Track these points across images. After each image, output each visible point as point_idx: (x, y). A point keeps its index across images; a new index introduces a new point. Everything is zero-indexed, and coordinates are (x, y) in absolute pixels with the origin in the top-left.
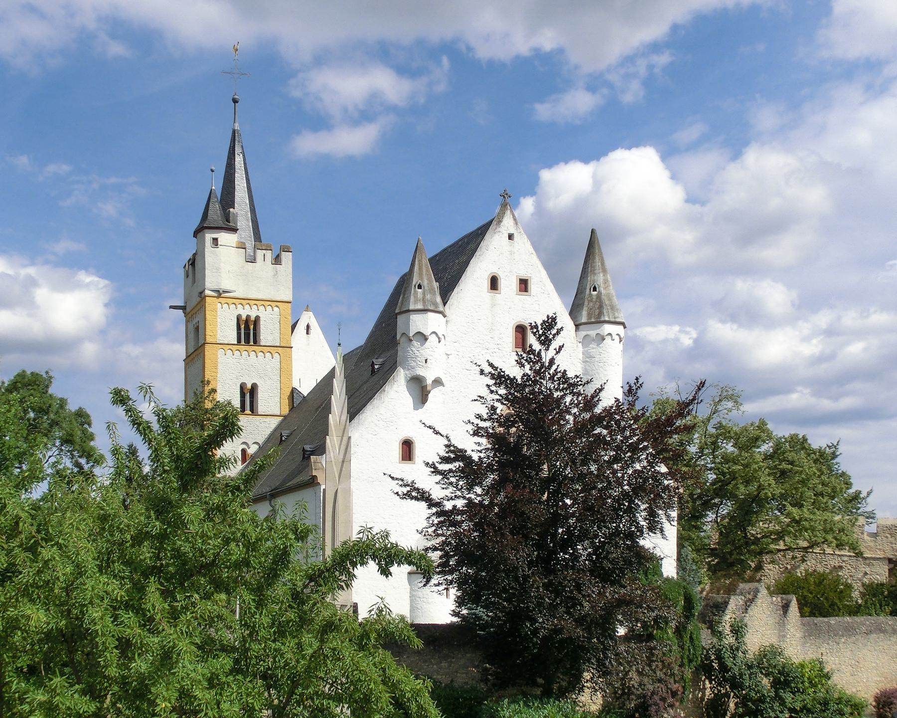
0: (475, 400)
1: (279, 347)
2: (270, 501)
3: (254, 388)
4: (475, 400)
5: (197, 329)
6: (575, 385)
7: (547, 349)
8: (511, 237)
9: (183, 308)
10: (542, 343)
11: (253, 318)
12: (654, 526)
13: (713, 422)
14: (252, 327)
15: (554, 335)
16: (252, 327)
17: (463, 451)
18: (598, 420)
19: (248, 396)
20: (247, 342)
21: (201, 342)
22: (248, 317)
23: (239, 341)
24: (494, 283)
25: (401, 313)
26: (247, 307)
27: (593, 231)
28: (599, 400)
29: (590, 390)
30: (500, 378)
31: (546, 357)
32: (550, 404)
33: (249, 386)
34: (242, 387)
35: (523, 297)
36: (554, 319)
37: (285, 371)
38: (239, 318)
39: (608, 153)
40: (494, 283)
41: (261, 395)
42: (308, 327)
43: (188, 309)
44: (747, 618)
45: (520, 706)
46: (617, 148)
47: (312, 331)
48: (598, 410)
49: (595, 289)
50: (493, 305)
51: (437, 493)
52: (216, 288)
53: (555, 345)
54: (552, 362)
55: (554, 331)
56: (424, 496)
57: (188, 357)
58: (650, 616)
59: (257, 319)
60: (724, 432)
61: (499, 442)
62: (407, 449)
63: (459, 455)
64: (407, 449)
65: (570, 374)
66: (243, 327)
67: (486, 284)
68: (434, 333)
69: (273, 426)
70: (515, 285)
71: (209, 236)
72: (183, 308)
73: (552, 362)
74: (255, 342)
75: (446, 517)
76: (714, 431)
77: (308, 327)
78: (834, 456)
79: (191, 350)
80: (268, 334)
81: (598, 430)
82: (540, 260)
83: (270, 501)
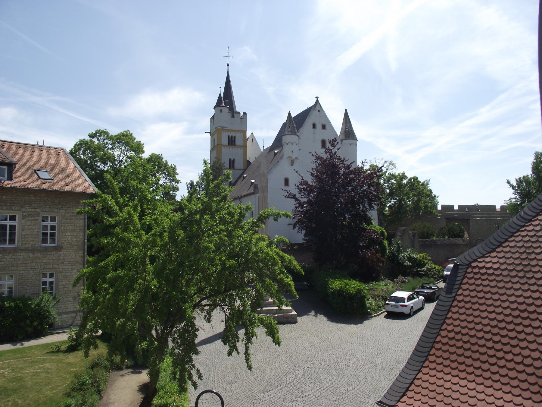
0: (247, 360)
3: (234, 160)
4: (247, 360)
6: (343, 161)
7: (334, 149)
8: (319, 111)
9: (210, 133)
10: (333, 146)
11: (234, 136)
12: (371, 207)
13: (388, 172)
14: (233, 139)
15: (336, 145)
16: (233, 139)
17: (307, 182)
18: (351, 172)
19: (232, 164)
20: (232, 144)
22: (232, 136)
24: (314, 126)
25: (284, 135)
26: (234, 133)
27: (346, 110)
28: (351, 166)
29: (348, 163)
30: (318, 158)
31: (334, 151)
32: (334, 166)
33: (232, 159)
34: (230, 160)
35: (324, 131)
36: (205, 160)
38: (229, 136)
40: (314, 126)
47: (253, 141)
48: (351, 169)
49: (347, 129)
50: (314, 133)
51: (298, 196)
53: (337, 147)
54: (336, 153)
55: (336, 143)
56: (294, 197)
57: (211, 149)
58: (377, 252)
60: (392, 176)
61: (318, 178)
62: (286, 182)
63: (305, 183)
64: (286, 182)
65: (341, 157)
66: (230, 139)
67: (311, 126)
68: (295, 142)
70: (321, 127)
72: (210, 133)
73: (336, 153)
74: (234, 145)
75: (301, 205)
76: (388, 176)
78: (427, 184)
79: (212, 147)
81: (351, 176)
82: (212, 336)
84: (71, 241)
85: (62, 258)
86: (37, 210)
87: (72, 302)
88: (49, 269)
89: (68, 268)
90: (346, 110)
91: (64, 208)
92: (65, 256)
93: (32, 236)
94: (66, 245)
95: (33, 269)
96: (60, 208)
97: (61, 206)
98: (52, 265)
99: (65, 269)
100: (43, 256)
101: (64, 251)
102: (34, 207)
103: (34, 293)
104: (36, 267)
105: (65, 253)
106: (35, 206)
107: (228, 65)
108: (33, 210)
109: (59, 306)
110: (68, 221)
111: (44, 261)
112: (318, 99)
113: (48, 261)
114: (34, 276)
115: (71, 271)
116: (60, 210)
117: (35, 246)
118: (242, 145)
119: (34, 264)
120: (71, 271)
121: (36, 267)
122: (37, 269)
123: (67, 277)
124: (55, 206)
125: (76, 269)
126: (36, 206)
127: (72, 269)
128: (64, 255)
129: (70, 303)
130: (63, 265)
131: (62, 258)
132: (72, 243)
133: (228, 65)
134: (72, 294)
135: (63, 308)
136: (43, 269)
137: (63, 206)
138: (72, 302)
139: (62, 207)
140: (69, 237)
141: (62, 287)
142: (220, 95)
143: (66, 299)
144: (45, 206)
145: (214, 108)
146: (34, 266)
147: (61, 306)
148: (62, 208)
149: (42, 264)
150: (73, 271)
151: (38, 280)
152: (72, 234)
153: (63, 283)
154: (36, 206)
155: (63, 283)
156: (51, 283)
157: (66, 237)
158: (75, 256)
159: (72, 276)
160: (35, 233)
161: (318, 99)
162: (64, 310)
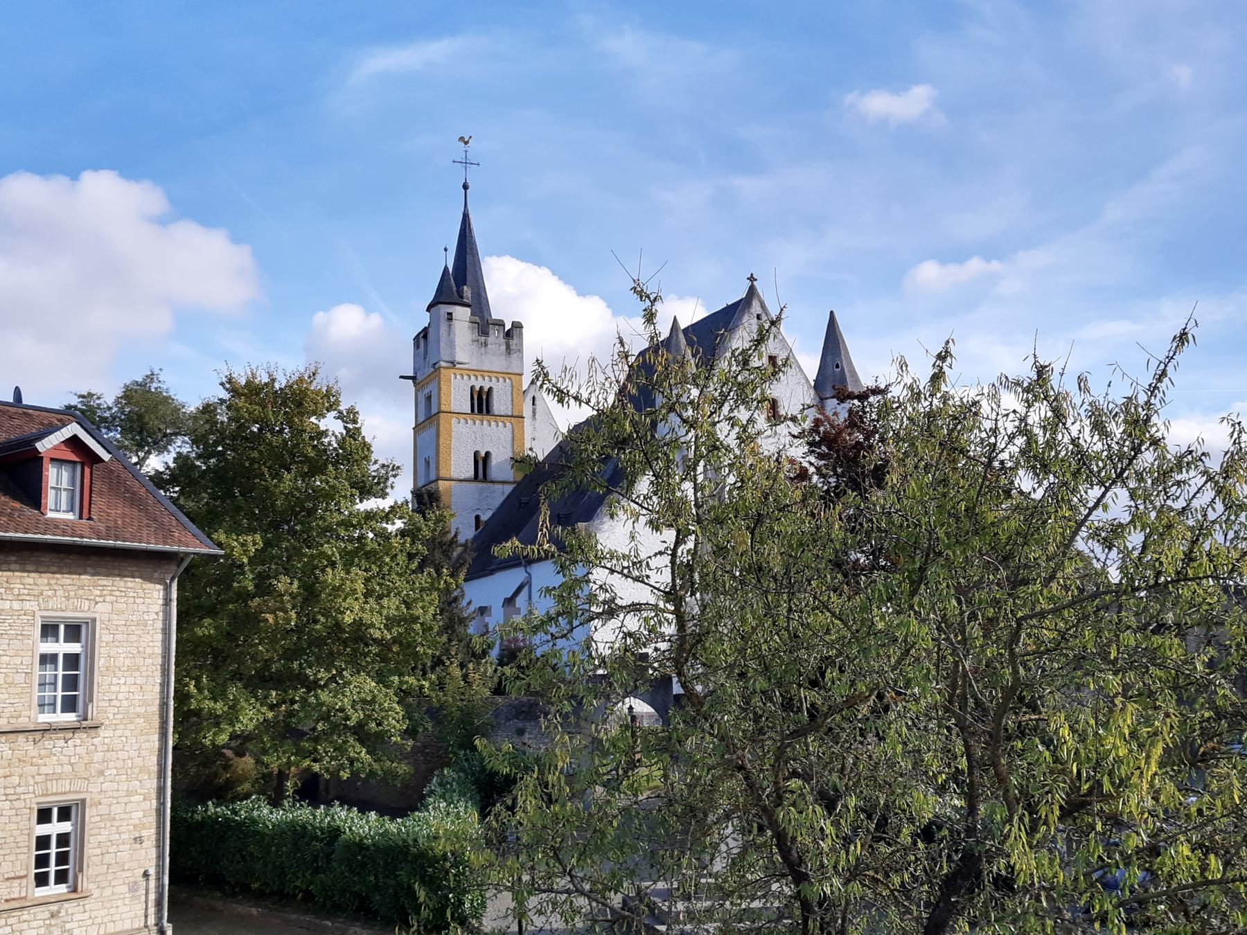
1: (512, 416)
2: (526, 567)
5: (429, 398)
9: (413, 378)
11: (486, 389)
14: (484, 397)
16: (484, 397)
20: (480, 411)
21: (434, 410)
22: (481, 388)
23: (472, 410)
27: (832, 312)
33: (483, 454)
34: (476, 454)
37: (517, 437)
38: (472, 388)
39: (571, 284)
41: (494, 461)
42: (534, 398)
43: (419, 378)
44: (532, 682)
45: (1021, 692)
46: (354, 303)
47: (536, 402)
49: (837, 366)
52: (450, 359)
59: (490, 389)
69: (507, 493)
71: (444, 309)
72: (413, 378)
74: (488, 412)
77: (534, 398)
79: (421, 419)
80: (500, 404)
83: (526, 567)
84: (125, 703)
85: (98, 756)
86: (27, 605)
87: (127, 901)
88: (61, 794)
89: (118, 790)
90: (832, 312)
91: (108, 599)
92: (108, 751)
93: (11, 690)
94: (111, 716)
95: (10, 797)
96: (98, 599)
97: (98, 593)
98: (68, 781)
99: (110, 794)
100: (43, 752)
101: (101, 732)
102: (19, 595)
103: (12, 875)
104: (19, 790)
105: (106, 741)
106: (23, 591)
107: (465, 187)
108: (16, 605)
109: (87, 915)
110: (119, 637)
111: (44, 770)
112: (755, 283)
113: (58, 769)
114: (14, 819)
115: (126, 799)
116: (97, 603)
117: (20, 720)
118: (510, 414)
119: (16, 780)
120: (126, 799)
121: (19, 790)
122: (22, 797)
123: (114, 819)
124: (81, 592)
125: (143, 791)
126: (26, 592)
127: (129, 793)
128: (106, 747)
129: (120, 903)
130: (102, 779)
131: (98, 756)
132: (132, 710)
133: (465, 187)
134: (128, 874)
135: (99, 920)
136: (43, 795)
137: (105, 592)
138: (127, 901)
139: (100, 596)
140: (124, 689)
141: (98, 851)
142: (446, 269)
143: (108, 892)
144: (50, 593)
145: (428, 310)
146: (14, 788)
147: (94, 914)
148: (101, 599)
149: (39, 779)
150: (132, 799)
151: (27, 832)
152: (130, 680)
153: (100, 838)
154: (26, 592)
155: (100, 838)
156: (63, 839)
157: (113, 688)
158: (139, 749)
159: (128, 816)
160: (20, 678)
161: (755, 283)
162: (103, 927)
